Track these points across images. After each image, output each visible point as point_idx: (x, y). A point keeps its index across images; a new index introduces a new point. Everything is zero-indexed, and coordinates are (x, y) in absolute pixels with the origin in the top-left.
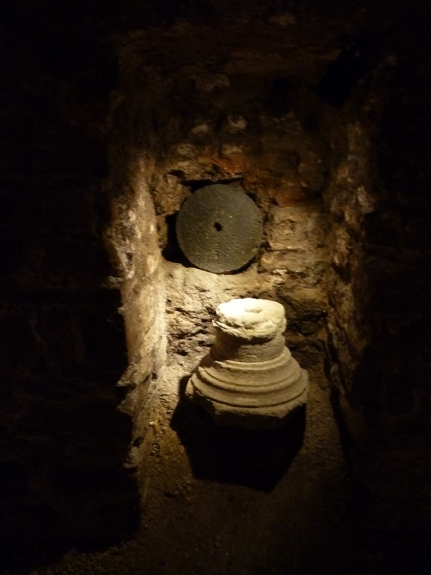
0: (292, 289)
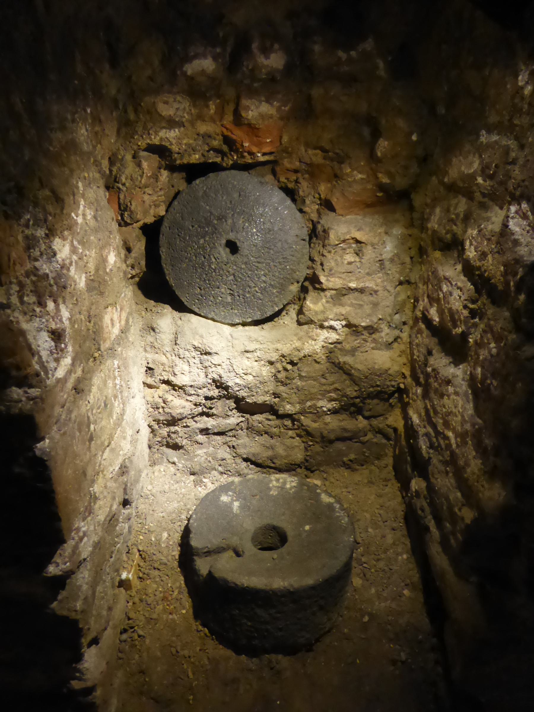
0: (353, 352)
